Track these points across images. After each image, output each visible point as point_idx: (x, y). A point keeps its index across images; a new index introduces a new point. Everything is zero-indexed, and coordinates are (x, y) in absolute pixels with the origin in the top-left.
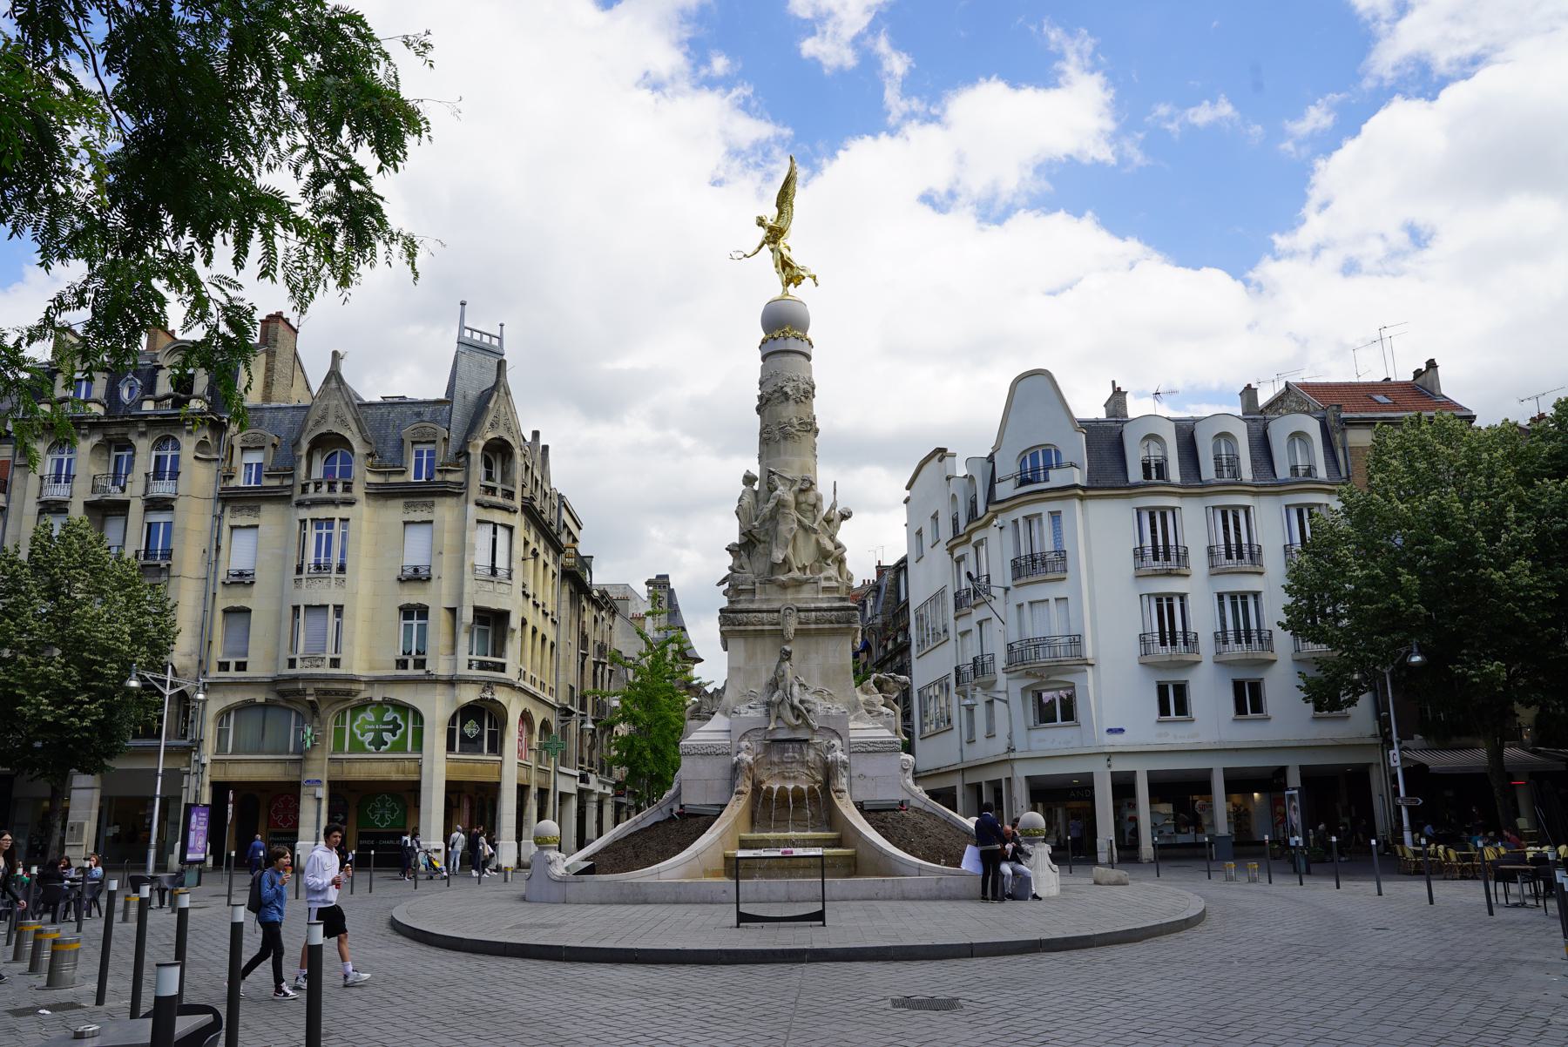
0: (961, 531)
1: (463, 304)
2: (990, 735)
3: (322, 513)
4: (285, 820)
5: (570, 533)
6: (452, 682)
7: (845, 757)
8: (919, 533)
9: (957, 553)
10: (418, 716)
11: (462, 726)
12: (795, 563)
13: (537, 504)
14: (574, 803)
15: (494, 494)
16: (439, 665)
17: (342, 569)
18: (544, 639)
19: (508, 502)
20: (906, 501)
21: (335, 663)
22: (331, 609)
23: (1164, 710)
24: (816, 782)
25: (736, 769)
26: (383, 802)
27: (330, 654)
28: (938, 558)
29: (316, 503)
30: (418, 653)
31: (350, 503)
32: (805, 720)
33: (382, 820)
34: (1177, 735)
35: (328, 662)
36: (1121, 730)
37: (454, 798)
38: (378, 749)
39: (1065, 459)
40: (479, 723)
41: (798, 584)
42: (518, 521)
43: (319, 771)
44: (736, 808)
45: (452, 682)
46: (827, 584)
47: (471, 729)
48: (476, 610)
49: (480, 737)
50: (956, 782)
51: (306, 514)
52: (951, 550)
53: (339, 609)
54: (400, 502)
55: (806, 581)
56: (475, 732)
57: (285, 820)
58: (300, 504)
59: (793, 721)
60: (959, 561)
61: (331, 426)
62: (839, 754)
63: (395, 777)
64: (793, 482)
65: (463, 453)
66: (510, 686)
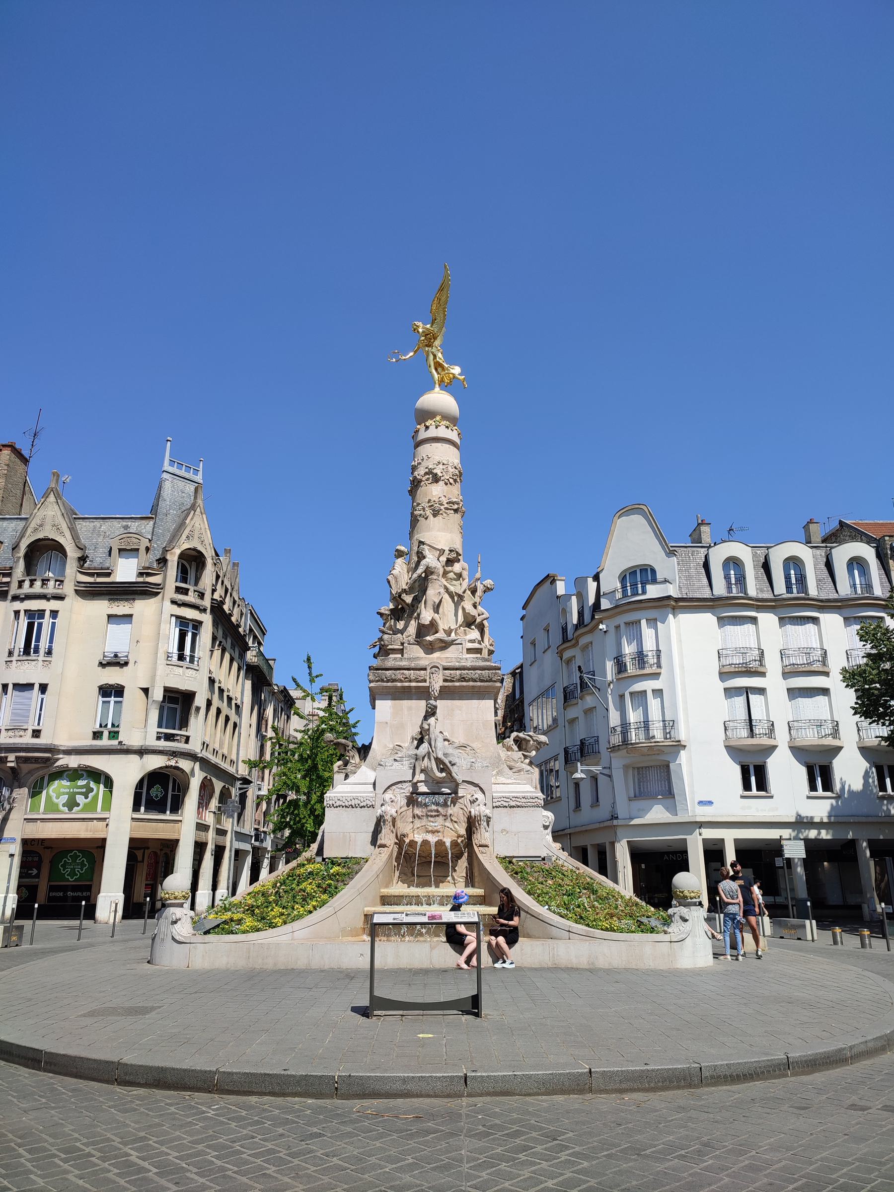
0: (570, 636)
3: (34, 605)
5: (255, 637)
6: (142, 752)
7: (488, 812)
8: (533, 644)
9: (567, 655)
10: (108, 782)
12: (442, 625)
13: (226, 607)
14: (249, 861)
15: (187, 594)
16: (131, 737)
17: (49, 652)
18: (227, 719)
19: (198, 602)
20: (522, 619)
22: (37, 687)
23: (747, 786)
24: (459, 836)
25: (379, 823)
26: (75, 857)
27: (32, 726)
28: (549, 660)
29: (29, 597)
30: (113, 725)
31: (61, 598)
32: (449, 773)
33: (73, 873)
34: (757, 809)
35: (30, 732)
36: (710, 803)
37: (139, 854)
38: (70, 809)
39: (660, 576)
41: (445, 645)
42: (207, 619)
44: (379, 860)
45: (142, 752)
46: (470, 646)
47: (156, 791)
48: (167, 690)
51: (17, 605)
52: (560, 654)
53: (43, 688)
55: (452, 643)
58: (15, 598)
59: (439, 775)
60: (569, 662)
61: (48, 532)
62: (482, 808)
64: (442, 552)
65: (163, 561)
66: (193, 757)
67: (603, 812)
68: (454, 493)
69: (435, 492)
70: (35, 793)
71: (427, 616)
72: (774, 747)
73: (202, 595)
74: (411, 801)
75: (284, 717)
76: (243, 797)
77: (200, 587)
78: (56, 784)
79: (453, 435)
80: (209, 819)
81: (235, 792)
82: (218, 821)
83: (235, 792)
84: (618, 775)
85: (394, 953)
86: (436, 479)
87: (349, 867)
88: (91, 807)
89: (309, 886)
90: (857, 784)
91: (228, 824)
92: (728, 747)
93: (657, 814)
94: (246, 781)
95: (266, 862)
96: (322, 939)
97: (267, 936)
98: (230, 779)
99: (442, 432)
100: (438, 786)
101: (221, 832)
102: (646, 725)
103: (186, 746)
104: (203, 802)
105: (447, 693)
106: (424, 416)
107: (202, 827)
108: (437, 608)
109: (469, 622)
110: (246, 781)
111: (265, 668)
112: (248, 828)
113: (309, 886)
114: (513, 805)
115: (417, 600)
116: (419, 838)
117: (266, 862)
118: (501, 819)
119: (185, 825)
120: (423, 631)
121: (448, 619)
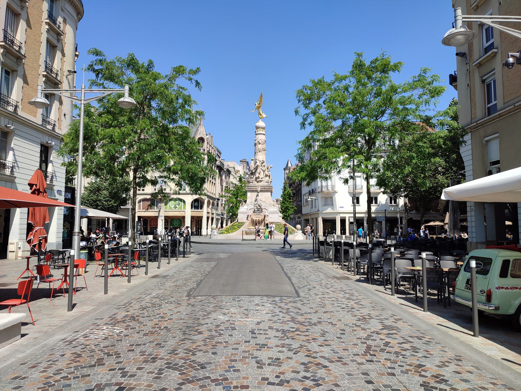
2: (315, 207)
4: (154, 225)
10: (184, 202)
12: (260, 177)
13: (210, 152)
26: (176, 220)
33: (176, 224)
41: (261, 181)
43: (163, 214)
44: (248, 223)
47: (196, 204)
50: (309, 217)
57: (154, 225)
63: (179, 215)
67: (316, 209)
68: (264, 146)
69: (260, 146)
70: (166, 205)
71: (257, 175)
72: (362, 192)
73: (204, 150)
74: (254, 212)
75: (228, 177)
76: (218, 204)
77: (203, 148)
78: (171, 202)
79: (264, 133)
80: (210, 211)
81: (215, 203)
82: (212, 211)
83: (215, 203)
84: (320, 199)
85: (246, 237)
86: (260, 144)
87: (242, 224)
88: (180, 208)
89: (235, 227)
90: (384, 202)
91: (214, 212)
92: (349, 192)
93: (329, 210)
94: (218, 199)
95: (225, 222)
96: (236, 235)
97: (229, 234)
98: (214, 199)
99: (261, 132)
100: (259, 209)
101: (213, 214)
102: (327, 186)
104: (208, 206)
105: (261, 191)
106: (257, 128)
107: (208, 213)
108: (259, 174)
109: (266, 176)
110: (218, 199)
111: (222, 166)
112: (219, 212)
113: (235, 227)
114: (273, 213)
115: (255, 171)
116: (255, 219)
117: (225, 222)
118: (270, 215)
119: (204, 212)
120: (256, 178)
121: (262, 175)
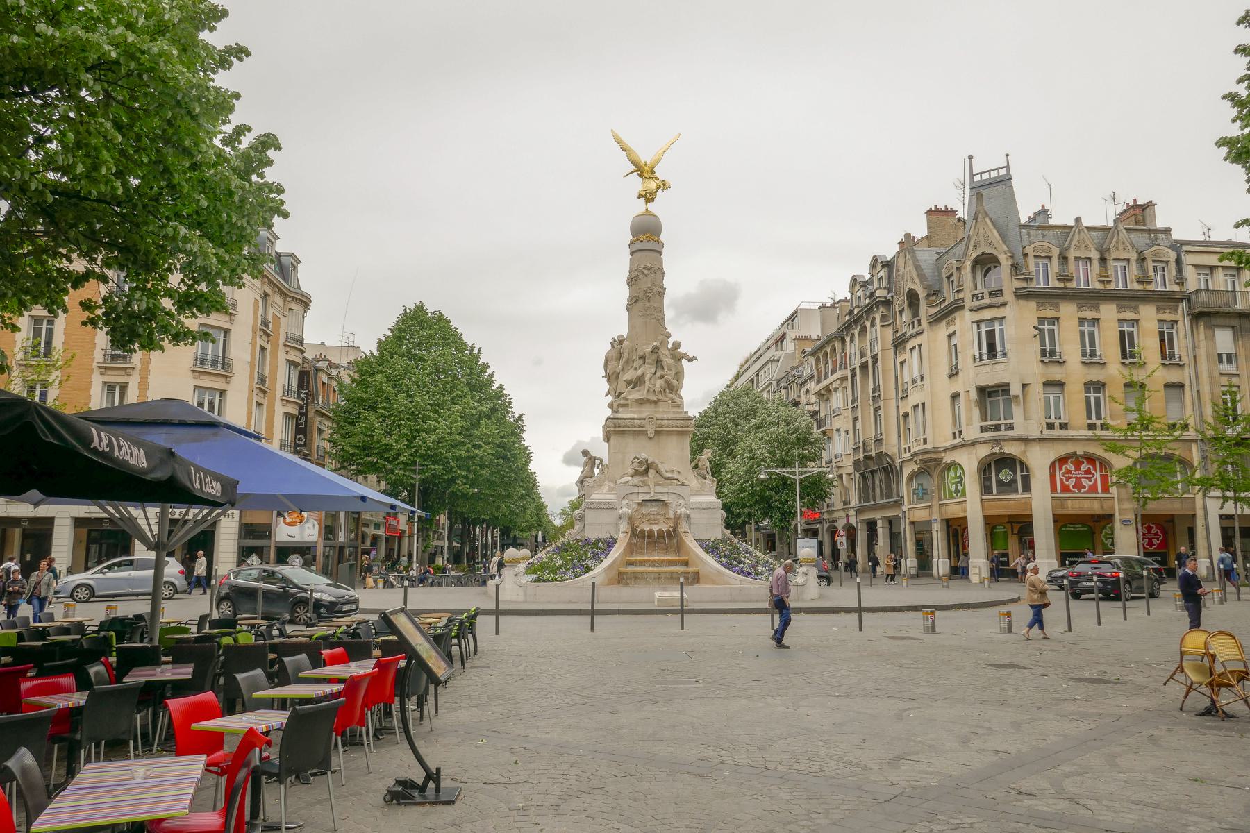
1: (971, 158)
10: (1025, 468)
11: (997, 474)
21: (925, 441)
40: (1002, 468)
47: (1005, 475)
49: (1014, 481)
53: (923, 404)
54: (944, 323)
56: (1009, 478)
103: (1010, 433)
